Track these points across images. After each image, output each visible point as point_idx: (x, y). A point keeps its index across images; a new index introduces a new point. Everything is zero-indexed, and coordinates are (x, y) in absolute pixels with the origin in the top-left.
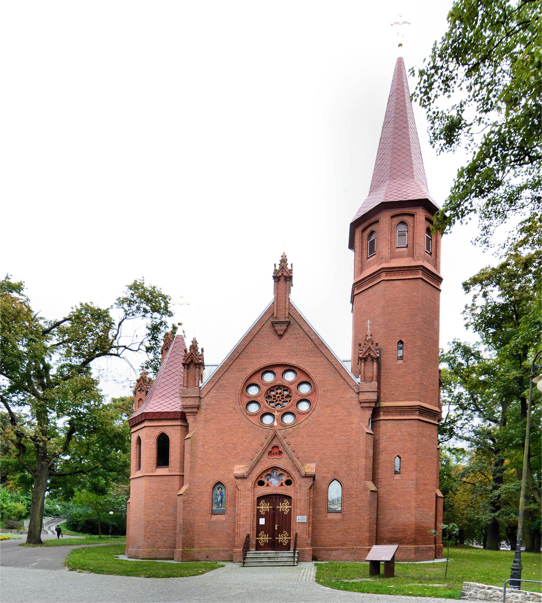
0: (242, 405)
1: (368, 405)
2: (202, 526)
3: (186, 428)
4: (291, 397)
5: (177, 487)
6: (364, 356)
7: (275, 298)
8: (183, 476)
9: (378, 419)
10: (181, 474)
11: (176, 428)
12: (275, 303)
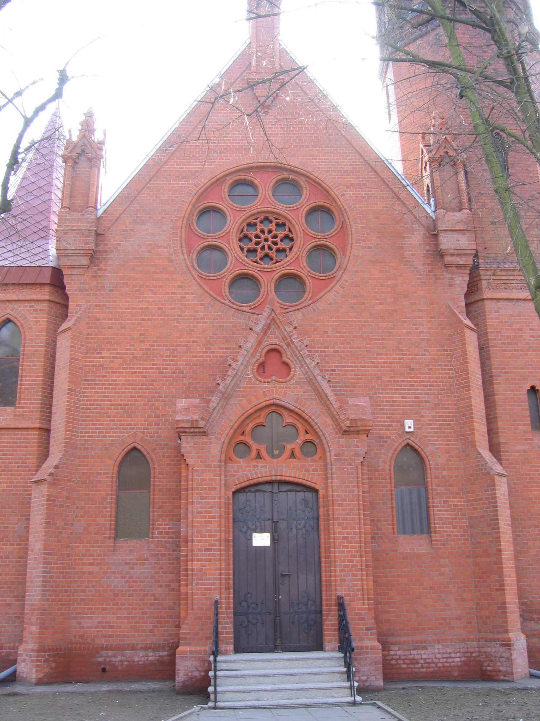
0: (189, 253)
1: (469, 251)
2: (90, 573)
3: (61, 305)
4: (292, 240)
5: (32, 461)
6: (437, 156)
7: (251, 37)
8: (48, 431)
9: (481, 297)
10: (44, 426)
11: (40, 306)
12: (254, 45)
